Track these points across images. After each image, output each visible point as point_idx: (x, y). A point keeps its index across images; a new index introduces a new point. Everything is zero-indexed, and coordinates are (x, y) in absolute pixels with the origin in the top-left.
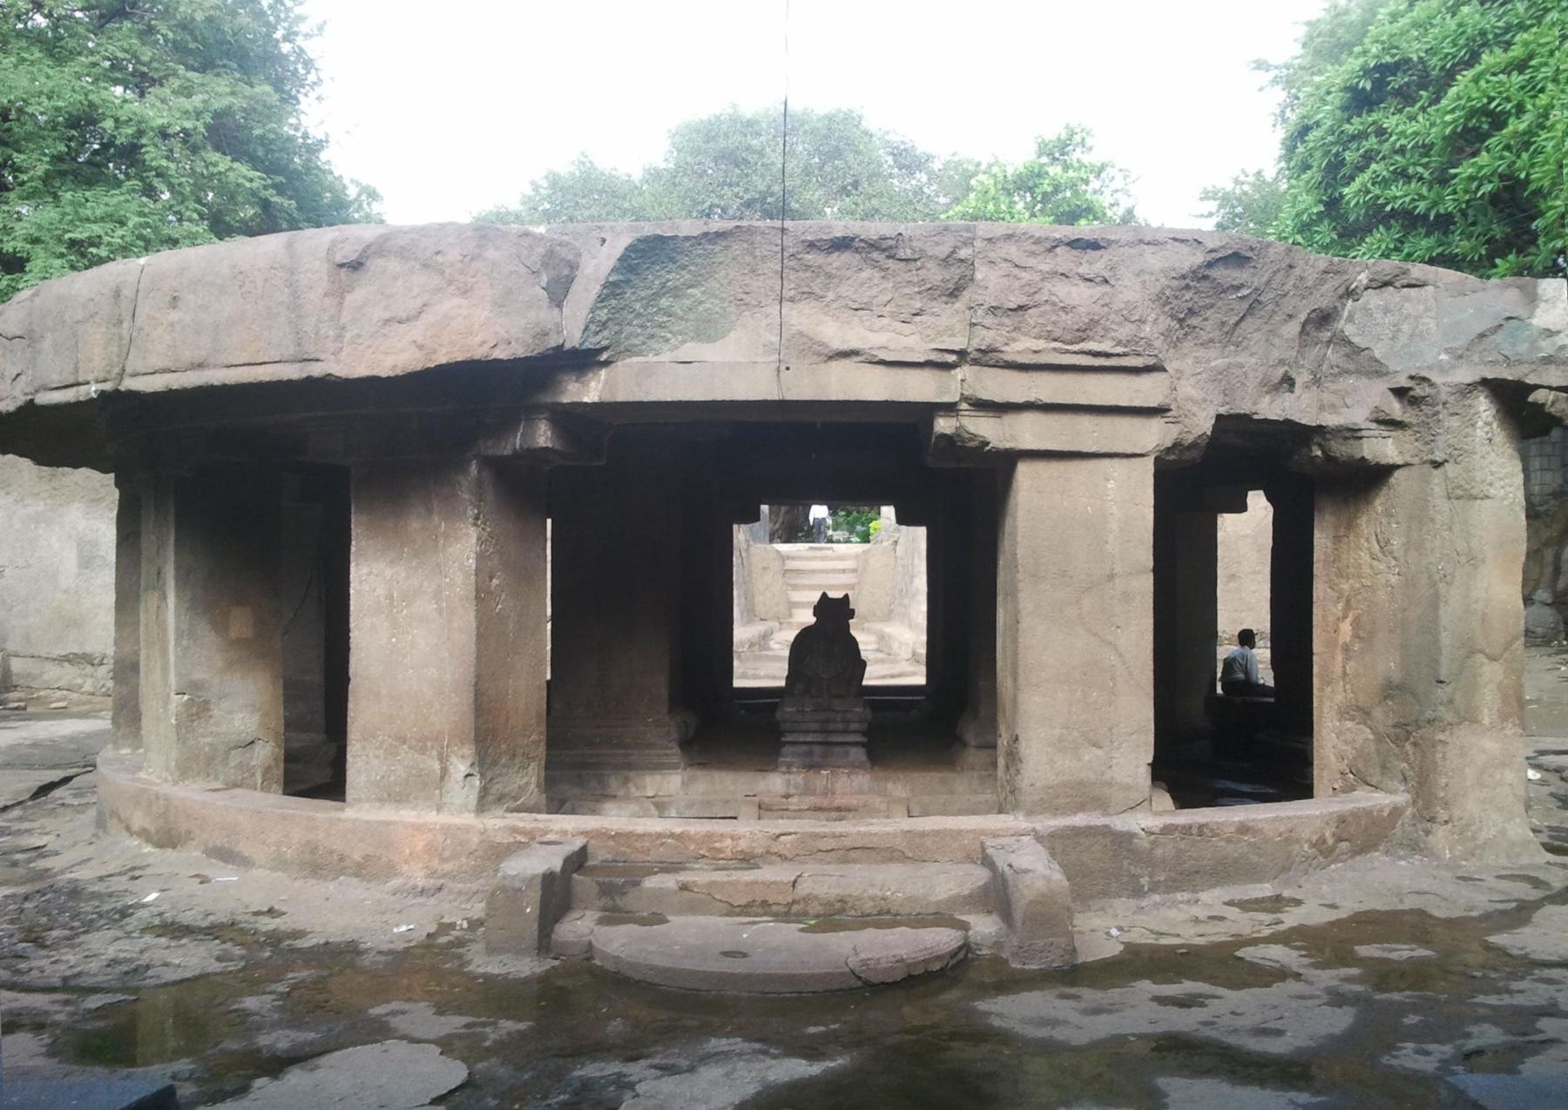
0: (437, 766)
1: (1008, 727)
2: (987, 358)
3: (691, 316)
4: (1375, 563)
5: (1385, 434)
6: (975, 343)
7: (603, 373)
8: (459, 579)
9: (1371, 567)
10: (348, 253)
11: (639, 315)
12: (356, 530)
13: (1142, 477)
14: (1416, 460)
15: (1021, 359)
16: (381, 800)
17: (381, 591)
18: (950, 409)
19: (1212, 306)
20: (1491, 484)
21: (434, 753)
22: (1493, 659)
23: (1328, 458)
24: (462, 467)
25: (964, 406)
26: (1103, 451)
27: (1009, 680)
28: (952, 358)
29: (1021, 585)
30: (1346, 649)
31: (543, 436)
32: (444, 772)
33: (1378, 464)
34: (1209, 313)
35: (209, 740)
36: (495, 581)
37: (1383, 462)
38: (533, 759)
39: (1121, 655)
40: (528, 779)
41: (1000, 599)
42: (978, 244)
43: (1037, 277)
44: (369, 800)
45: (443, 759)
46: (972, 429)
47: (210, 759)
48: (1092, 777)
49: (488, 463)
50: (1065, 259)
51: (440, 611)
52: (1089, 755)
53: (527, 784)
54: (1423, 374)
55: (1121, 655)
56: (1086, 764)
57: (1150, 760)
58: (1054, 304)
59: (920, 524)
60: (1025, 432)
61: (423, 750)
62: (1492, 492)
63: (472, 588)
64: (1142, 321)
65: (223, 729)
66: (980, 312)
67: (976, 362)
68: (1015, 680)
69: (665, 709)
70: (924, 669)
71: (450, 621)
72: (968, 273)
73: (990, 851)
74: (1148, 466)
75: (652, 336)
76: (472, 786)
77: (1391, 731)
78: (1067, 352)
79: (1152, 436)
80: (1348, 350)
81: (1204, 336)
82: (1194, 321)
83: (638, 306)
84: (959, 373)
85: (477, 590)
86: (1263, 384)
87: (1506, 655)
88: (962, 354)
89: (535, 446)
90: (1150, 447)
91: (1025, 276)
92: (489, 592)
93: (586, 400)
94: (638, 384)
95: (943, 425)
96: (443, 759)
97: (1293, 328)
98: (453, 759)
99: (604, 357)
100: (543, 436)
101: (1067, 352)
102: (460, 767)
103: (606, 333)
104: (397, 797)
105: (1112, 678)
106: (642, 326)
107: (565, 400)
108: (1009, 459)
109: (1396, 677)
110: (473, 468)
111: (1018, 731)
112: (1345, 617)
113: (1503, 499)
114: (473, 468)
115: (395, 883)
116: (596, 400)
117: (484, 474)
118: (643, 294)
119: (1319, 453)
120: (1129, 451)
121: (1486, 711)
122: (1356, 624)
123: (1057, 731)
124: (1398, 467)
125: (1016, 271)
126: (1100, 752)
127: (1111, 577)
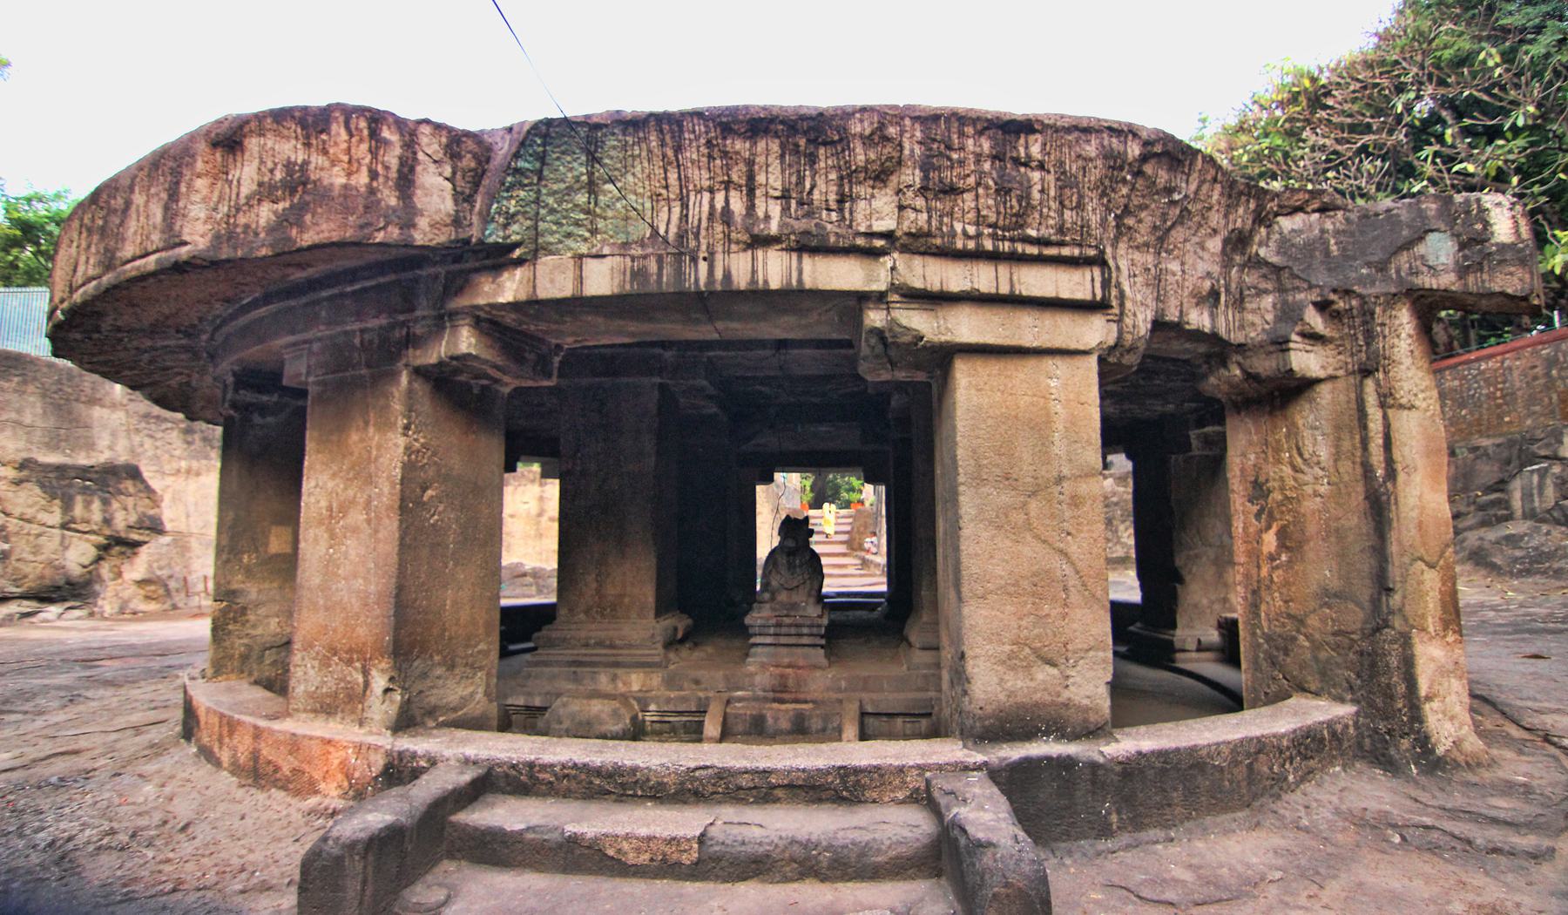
0: (361, 679)
1: (952, 643)
2: (918, 244)
3: (610, 213)
4: (1299, 475)
6: (905, 226)
7: (519, 273)
8: (386, 490)
9: (1295, 479)
11: (552, 211)
12: (310, 446)
13: (1087, 373)
14: (1341, 373)
16: (314, 711)
17: (324, 504)
18: (880, 298)
19: (1147, 207)
21: (358, 665)
22: (1431, 566)
23: (1250, 376)
24: (394, 376)
25: (896, 297)
26: (1048, 345)
27: (952, 594)
28: (879, 243)
29: (961, 488)
30: (1272, 558)
31: (466, 341)
32: (367, 684)
34: (1143, 215)
35: (245, 641)
36: (430, 492)
38: (481, 668)
39: (1073, 564)
41: (939, 508)
44: (305, 711)
45: (366, 672)
46: (904, 322)
47: (245, 658)
48: (1048, 698)
51: (369, 521)
52: (1044, 674)
53: (472, 694)
55: (1073, 564)
56: (1037, 684)
57: (1109, 678)
60: (965, 326)
61: (350, 662)
62: (1417, 403)
63: (397, 498)
65: (259, 631)
66: (910, 194)
67: (905, 249)
68: (959, 592)
69: (652, 614)
70: (885, 580)
71: (376, 531)
72: (895, 154)
73: (936, 794)
74: (1093, 361)
75: (569, 235)
76: (392, 701)
77: (1330, 639)
79: (1095, 332)
80: (1264, 270)
81: (1140, 240)
83: (550, 200)
84: (887, 261)
85: (402, 499)
86: (1193, 295)
88: (888, 235)
89: (459, 352)
90: (1093, 344)
92: (420, 504)
93: (501, 300)
94: (552, 281)
95: (875, 318)
96: (366, 672)
97: (1215, 244)
98: (374, 672)
99: (517, 253)
100: (466, 341)
102: (379, 682)
103: (515, 227)
104: (326, 707)
105: (1065, 589)
106: (556, 223)
107: (481, 301)
108: (945, 356)
109: (1335, 584)
110: (404, 379)
111: (965, 648)
112: (1269, 527)
113: (1426, 410)
114: (404, 379)
115: (313, 801)
116: (511, 299)
117: (416, 385)
118: (555, 187)
119: (1238, 372)
120: (1073, 346)
122: (1282, 535)
123: (1007, 648)
124: (1318, 381)
126: (1054, 671)
127: (1060, 480)
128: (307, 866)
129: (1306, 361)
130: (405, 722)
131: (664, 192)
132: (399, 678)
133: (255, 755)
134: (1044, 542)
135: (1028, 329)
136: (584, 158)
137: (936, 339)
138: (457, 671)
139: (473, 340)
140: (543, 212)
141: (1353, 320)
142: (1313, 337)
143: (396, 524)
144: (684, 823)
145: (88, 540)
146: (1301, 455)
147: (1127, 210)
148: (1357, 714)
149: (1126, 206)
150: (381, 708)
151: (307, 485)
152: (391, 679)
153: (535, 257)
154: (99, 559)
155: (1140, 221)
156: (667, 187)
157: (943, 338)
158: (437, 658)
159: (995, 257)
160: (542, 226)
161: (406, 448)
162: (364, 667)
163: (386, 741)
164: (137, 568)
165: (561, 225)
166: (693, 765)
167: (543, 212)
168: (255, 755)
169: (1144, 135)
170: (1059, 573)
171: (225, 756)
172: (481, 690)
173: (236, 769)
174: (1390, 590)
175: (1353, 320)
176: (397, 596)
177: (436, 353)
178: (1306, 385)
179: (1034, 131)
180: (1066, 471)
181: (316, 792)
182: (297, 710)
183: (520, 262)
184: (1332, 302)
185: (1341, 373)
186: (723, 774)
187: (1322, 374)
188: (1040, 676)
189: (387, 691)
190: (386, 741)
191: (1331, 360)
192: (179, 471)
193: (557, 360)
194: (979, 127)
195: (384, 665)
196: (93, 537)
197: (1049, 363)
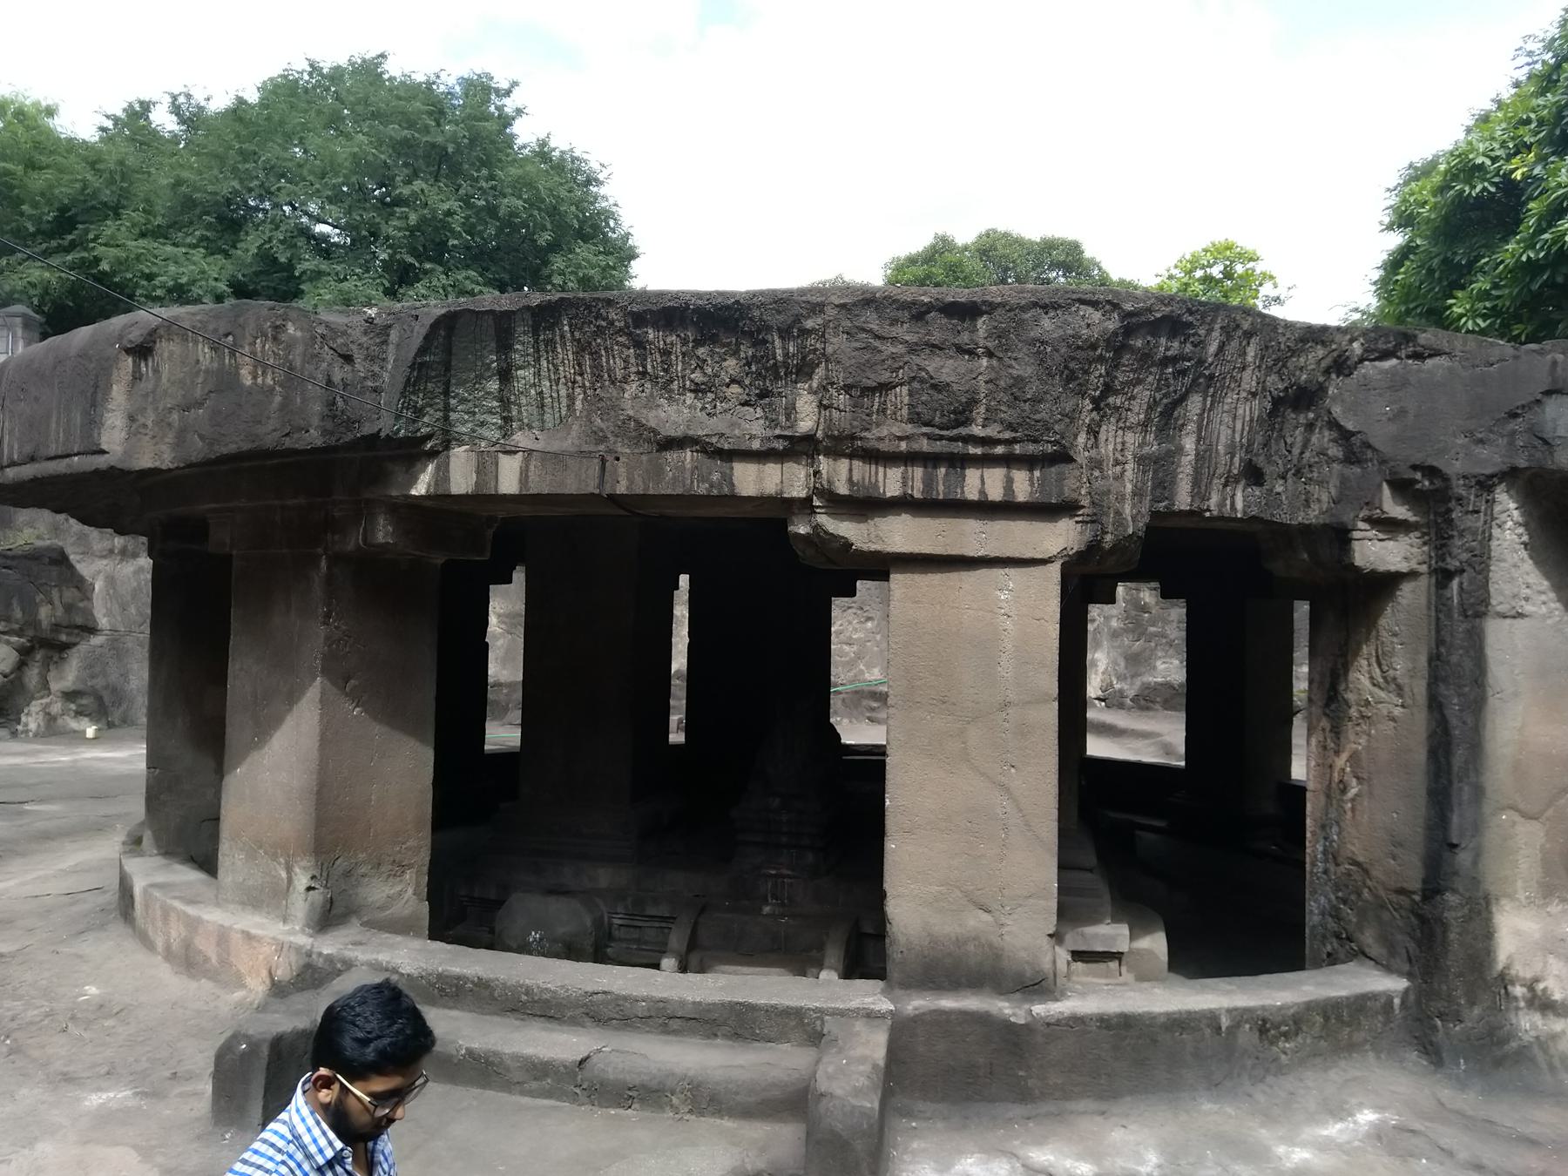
0: (284, 875)
2: (842, 445)
4: (1376, 690)
5: (1381, 536)
10: (135, 336)
11: (463, 401)
12: (234, 625)
15: (884, 447)
16: (243, 903)
20: (1527, 599)
31: (383, 532)
33: (1373, 572)
37: (1382, 568)
38: (410, 866)
40: (404, 892)
42: (831, 312)
43: (900, 349)
45: (289, 870)
49: (336, 559)
50: (939, 329)
53: (400, 894)
54: (1431, 462)
58: (922, 381)
59: (1086, 612)
61: (274, 857)
62: (1528, 608)
64: (1036, 401)
74: (1054, 570)
75: (482, 424)
78: (941, 438)
79: (1061, 537)
82: (241, 320)
87: (1550, 812)
91: (888, 349)
96: (289, 870)
100: (383, 532)
101: (941, 438)
102: (302, 880)
105: (1005, 828)
106: (467, 413)
120: (1028, 555)
121: (1519, 884)
125: (877, 343)
126: (986, 917)
127: (1006, 705)
128: (220, 1058)
129: (1376, 552)
130: (328, 918)
131: (579, 378)
132: (324, 874)
133: (188, 945)
134: (983, 774)
135: (972, 536)
136: (493, 345)
137: (865, 547)
138: (383, 869)
139: (390, 528)
140: (453, 402)
141: (1434, 502)
142: (1390, 527)
143: (317, 718)
144: (561, 1045)
145: (8, 643)
146: (1380, 665)
147: (1108, 389)
148: (1407, 991)
149: (1106, 384)
150: (300, 905)
151: (234, 668)
152: (313, 877)
153: (447, 448)
154: (21, 665)
155: (1133, 398)
156: (581, 375)
157: (873, 547)
158: (362, 856)
159: (929, 460)
160: (453, 416)
161: (327, 638)
162: (287, 863)
163: (304, 940)
164: (69, 675)
165: (474, 413)
166: (590, 989)
167: (453, 402)
168: (188, 945)
169: (1128, 307)
170: (999, 811)
171: (160, 943)
172: (410, 891)
173: (169, 955)
174: (1455, 846)
175: (1434, 502)
176: (318, 792)
177: (353, 541)
178: (1385, 583)
179: (981, 314)
180: (1012, 696)
181: (244, 986)
182: (226, 900)
183: (433, 454)
184: (1417, 482)
185: (1424, 568)
186: (619, 1000)
187: (1403, 567)
188: (972, 923)
189: (309, 889)
190: (304, 940)
191: (1415, 550)
192: (111, 551)
193: (490, 533)
194: (914, 311)
195: (304, 863)
196: (14, 639)
197: (998, 573)
